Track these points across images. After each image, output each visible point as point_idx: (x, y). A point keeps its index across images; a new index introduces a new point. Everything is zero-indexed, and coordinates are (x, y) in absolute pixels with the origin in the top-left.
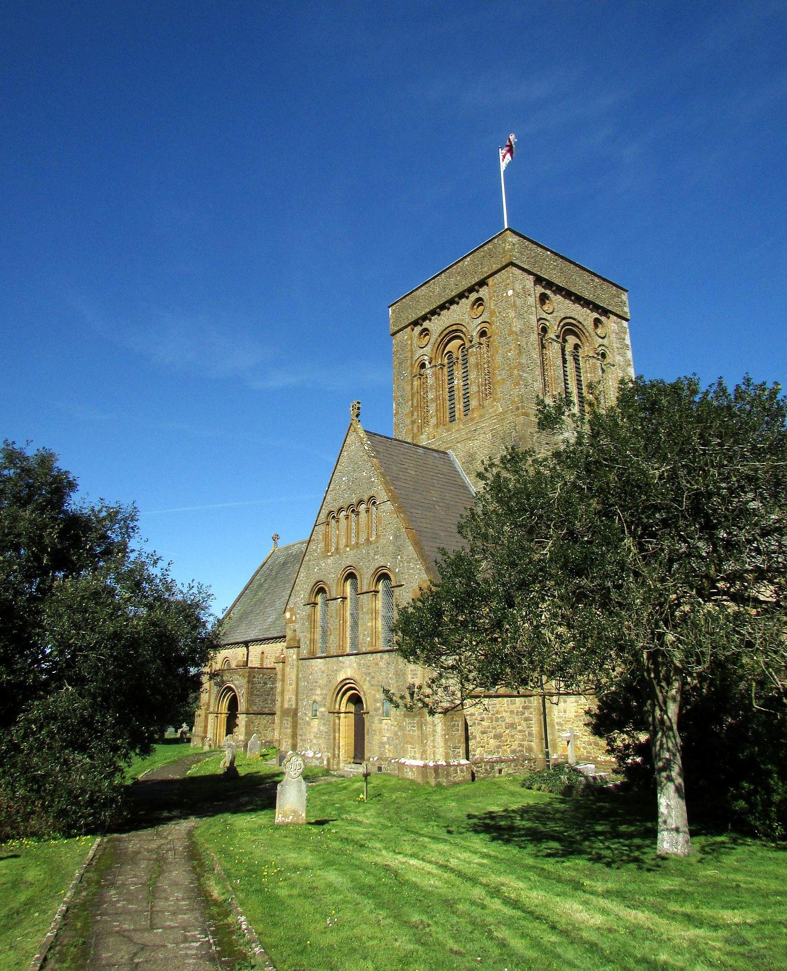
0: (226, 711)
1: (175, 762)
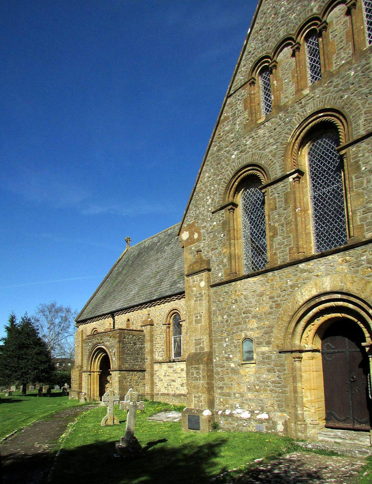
0: (98, 370)
1: (52, 416)
